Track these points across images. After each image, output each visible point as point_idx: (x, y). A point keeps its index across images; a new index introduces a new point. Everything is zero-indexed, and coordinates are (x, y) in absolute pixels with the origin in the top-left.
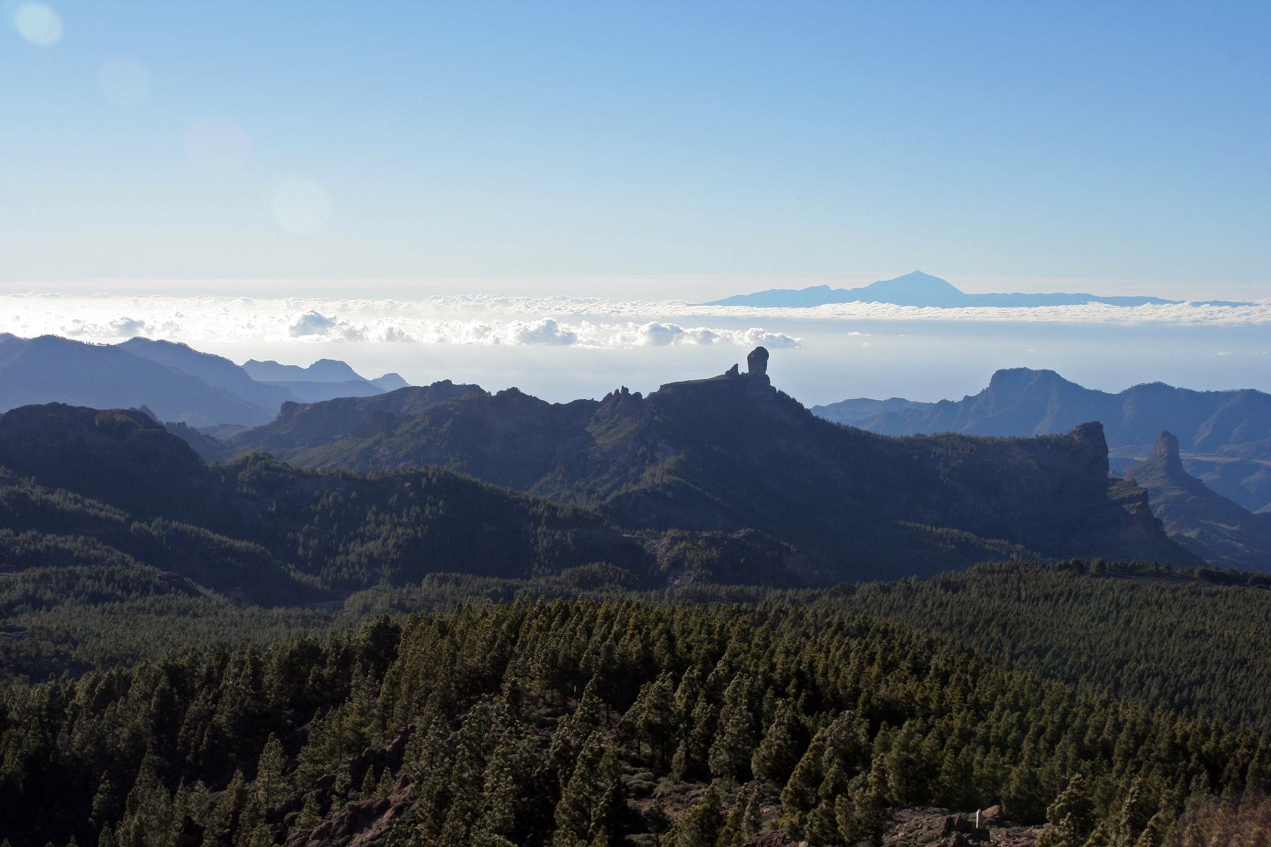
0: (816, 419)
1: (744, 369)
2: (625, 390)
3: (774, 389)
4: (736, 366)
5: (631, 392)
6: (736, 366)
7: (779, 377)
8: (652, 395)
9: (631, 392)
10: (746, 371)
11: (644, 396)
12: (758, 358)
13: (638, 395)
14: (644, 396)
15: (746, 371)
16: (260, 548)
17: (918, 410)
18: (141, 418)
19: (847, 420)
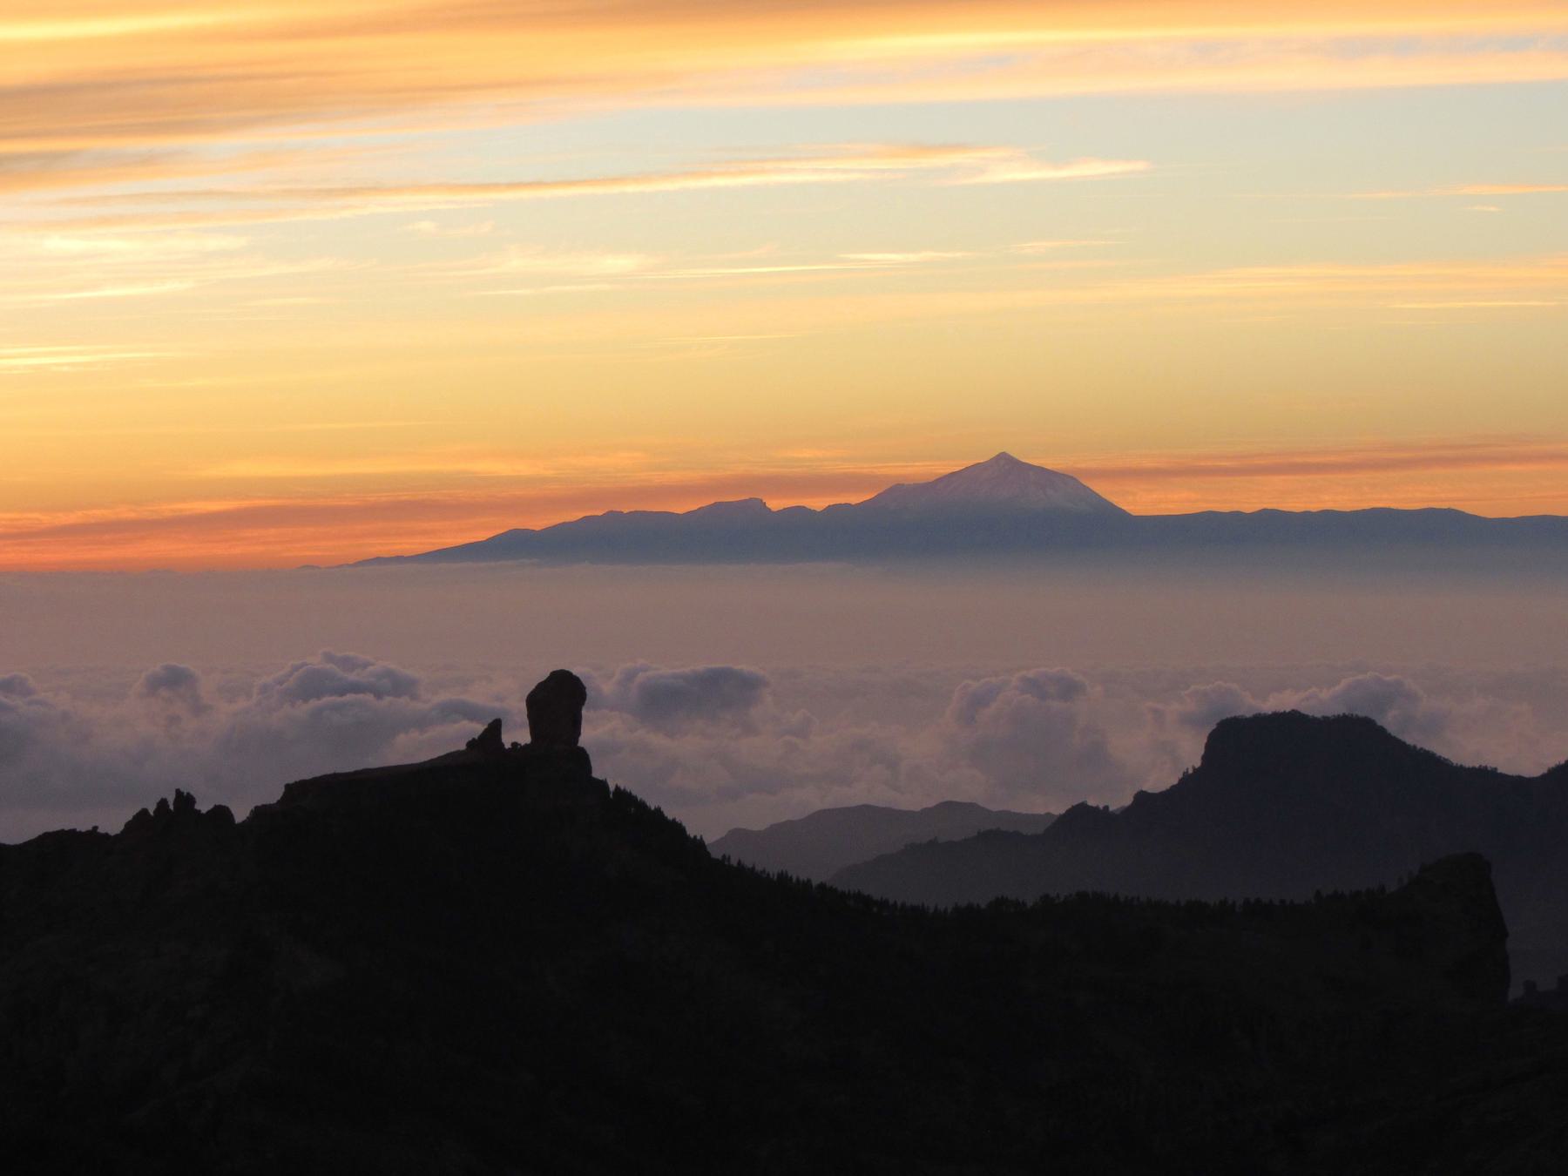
0: (722, 865)
1: (518, 734)
2: (184, 800)
3: (603, 785)
4: (495, 727)
5: (203, 807)
6: (495, 727)
7: (612, 743)
8: (260, 813)
9: (203, 807)
10: (524, 737)
11: (241, 814)
12: (559, 699)
13: (221, 813)
14: (241, 814)
15: (524, 737)
16: (1140, 166)
17: (999, 839)
18: (1265, 510)
19: (814, 870)
